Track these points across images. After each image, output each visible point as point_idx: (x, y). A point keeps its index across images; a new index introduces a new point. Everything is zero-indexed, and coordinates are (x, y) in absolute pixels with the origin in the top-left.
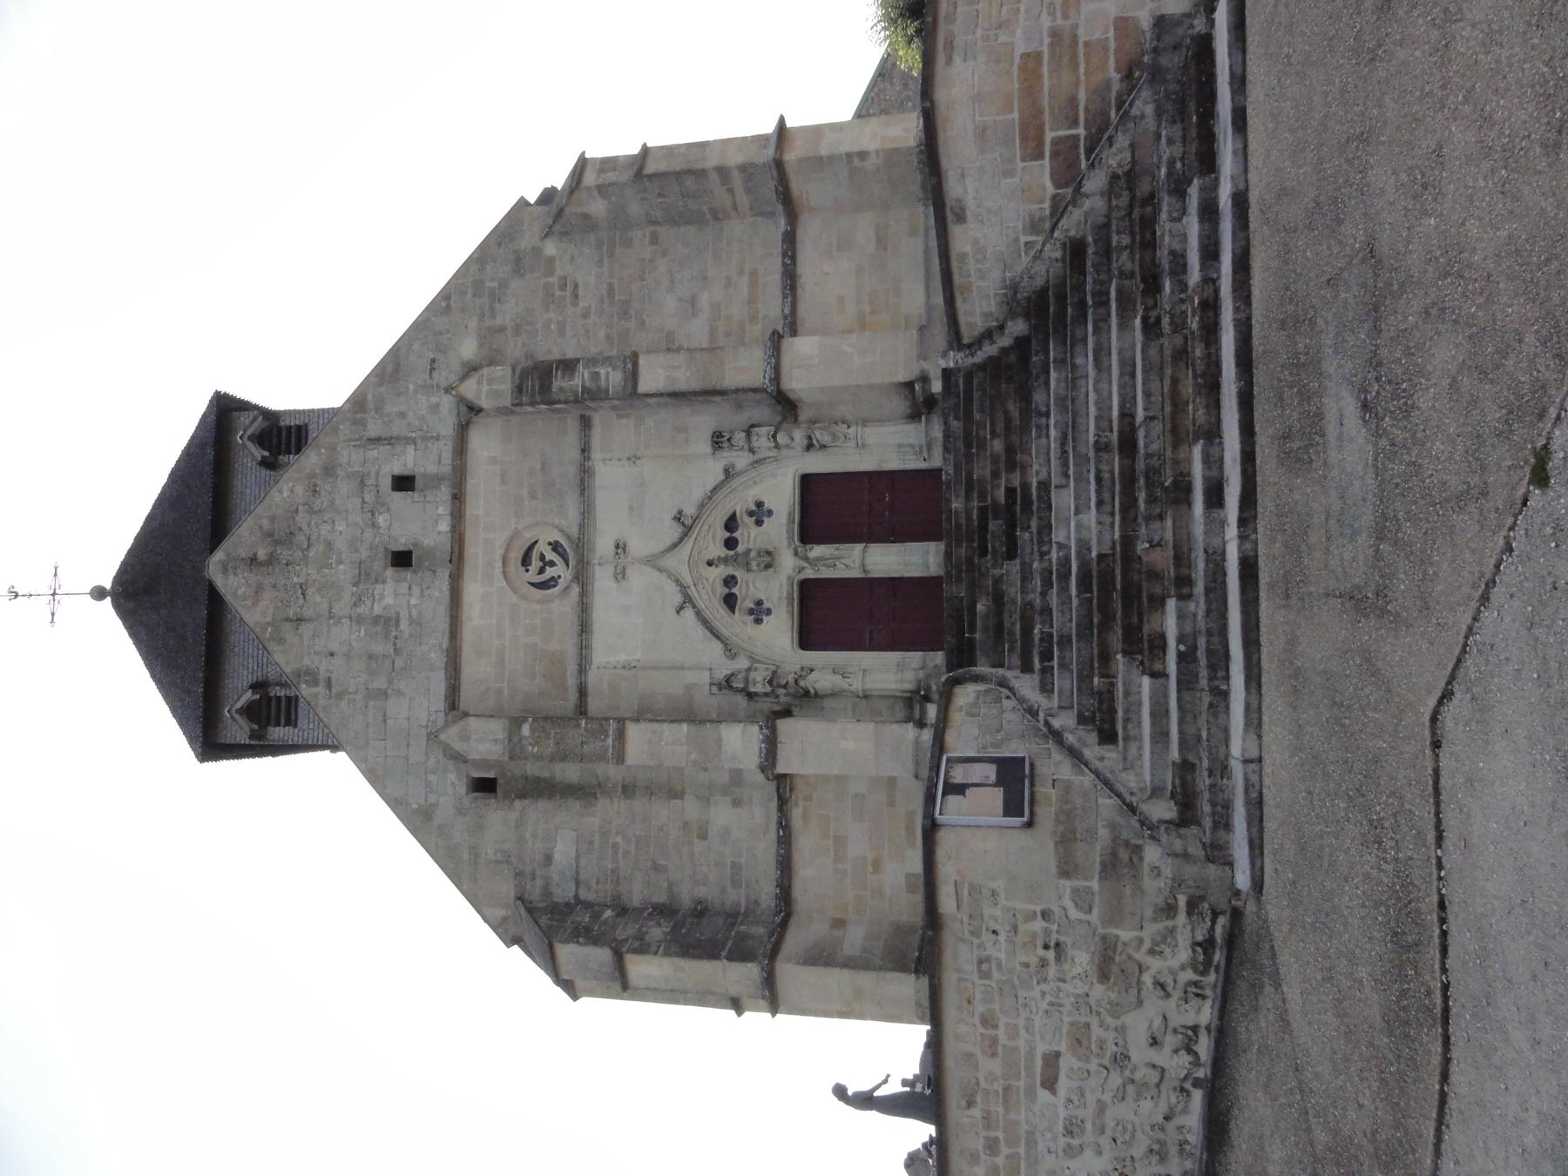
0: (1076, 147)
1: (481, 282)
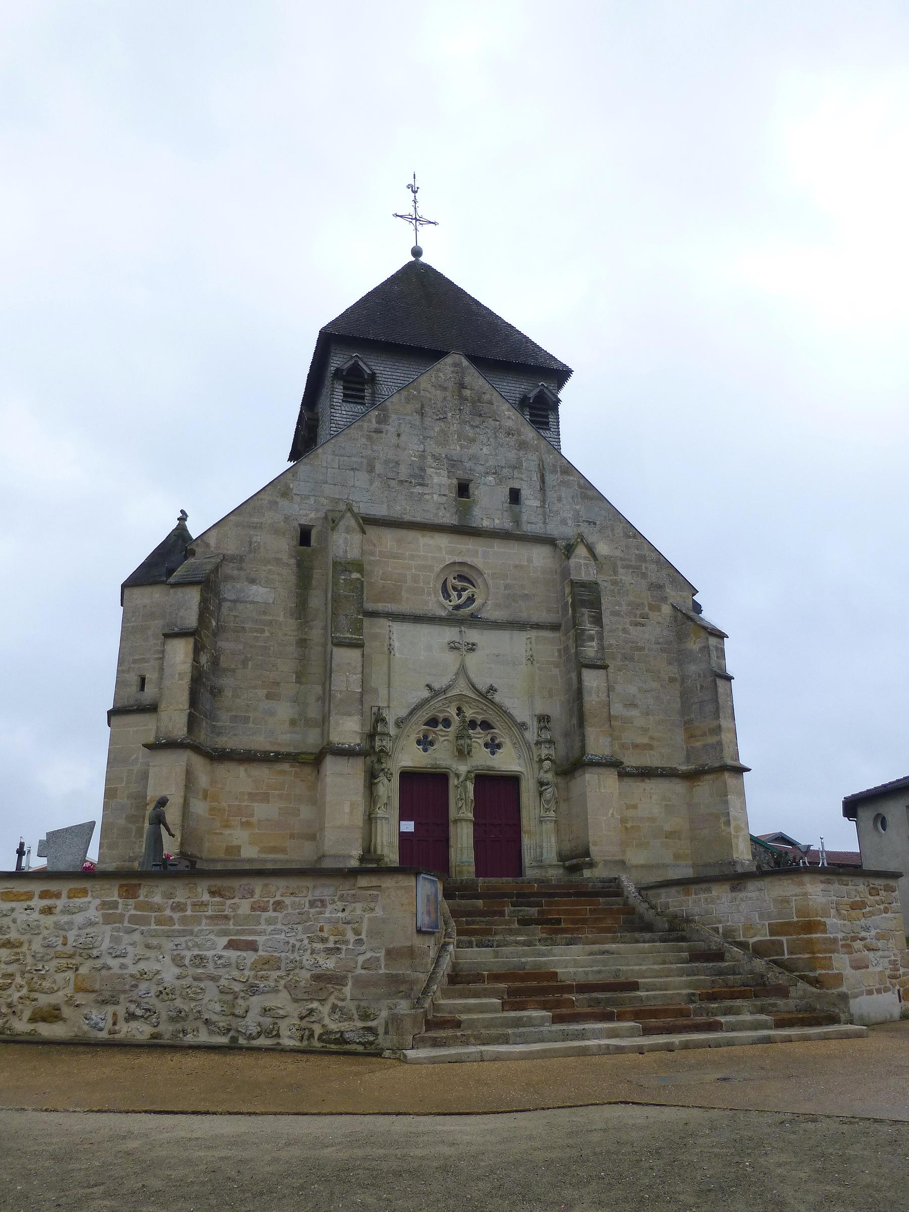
0: (778, 955)
1: (645, 561)
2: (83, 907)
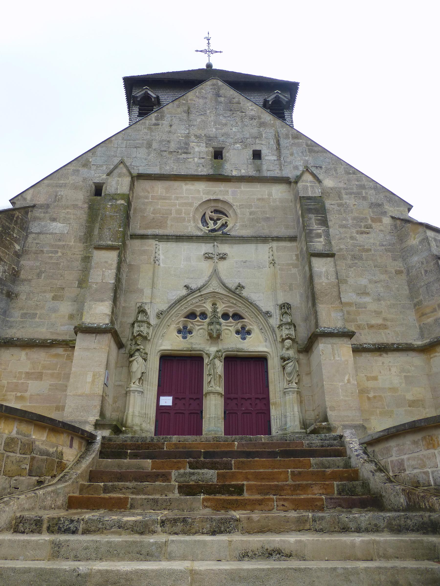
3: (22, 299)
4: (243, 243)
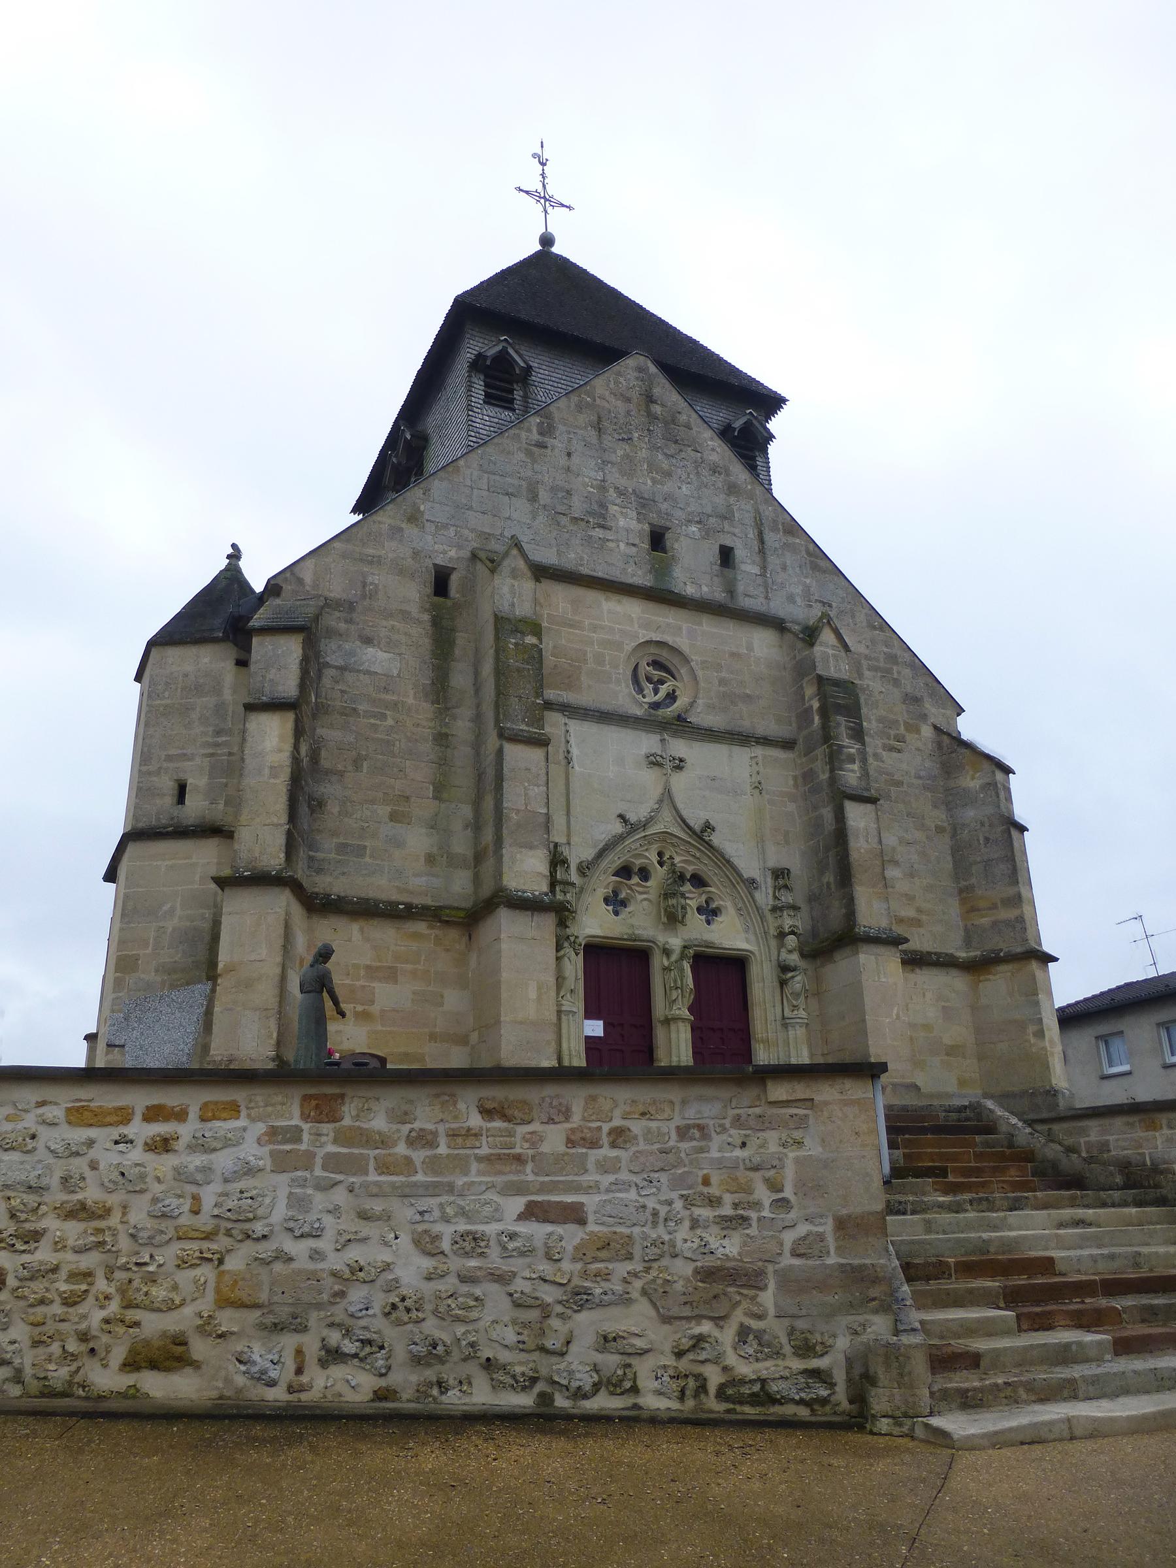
1: (897, 663)
2: (233, 1138)
3: (332, 814)
4: (709, 741)
